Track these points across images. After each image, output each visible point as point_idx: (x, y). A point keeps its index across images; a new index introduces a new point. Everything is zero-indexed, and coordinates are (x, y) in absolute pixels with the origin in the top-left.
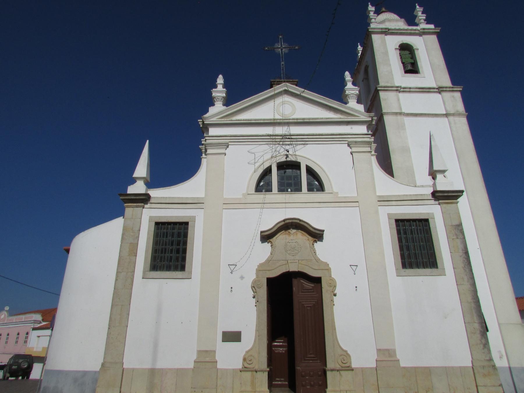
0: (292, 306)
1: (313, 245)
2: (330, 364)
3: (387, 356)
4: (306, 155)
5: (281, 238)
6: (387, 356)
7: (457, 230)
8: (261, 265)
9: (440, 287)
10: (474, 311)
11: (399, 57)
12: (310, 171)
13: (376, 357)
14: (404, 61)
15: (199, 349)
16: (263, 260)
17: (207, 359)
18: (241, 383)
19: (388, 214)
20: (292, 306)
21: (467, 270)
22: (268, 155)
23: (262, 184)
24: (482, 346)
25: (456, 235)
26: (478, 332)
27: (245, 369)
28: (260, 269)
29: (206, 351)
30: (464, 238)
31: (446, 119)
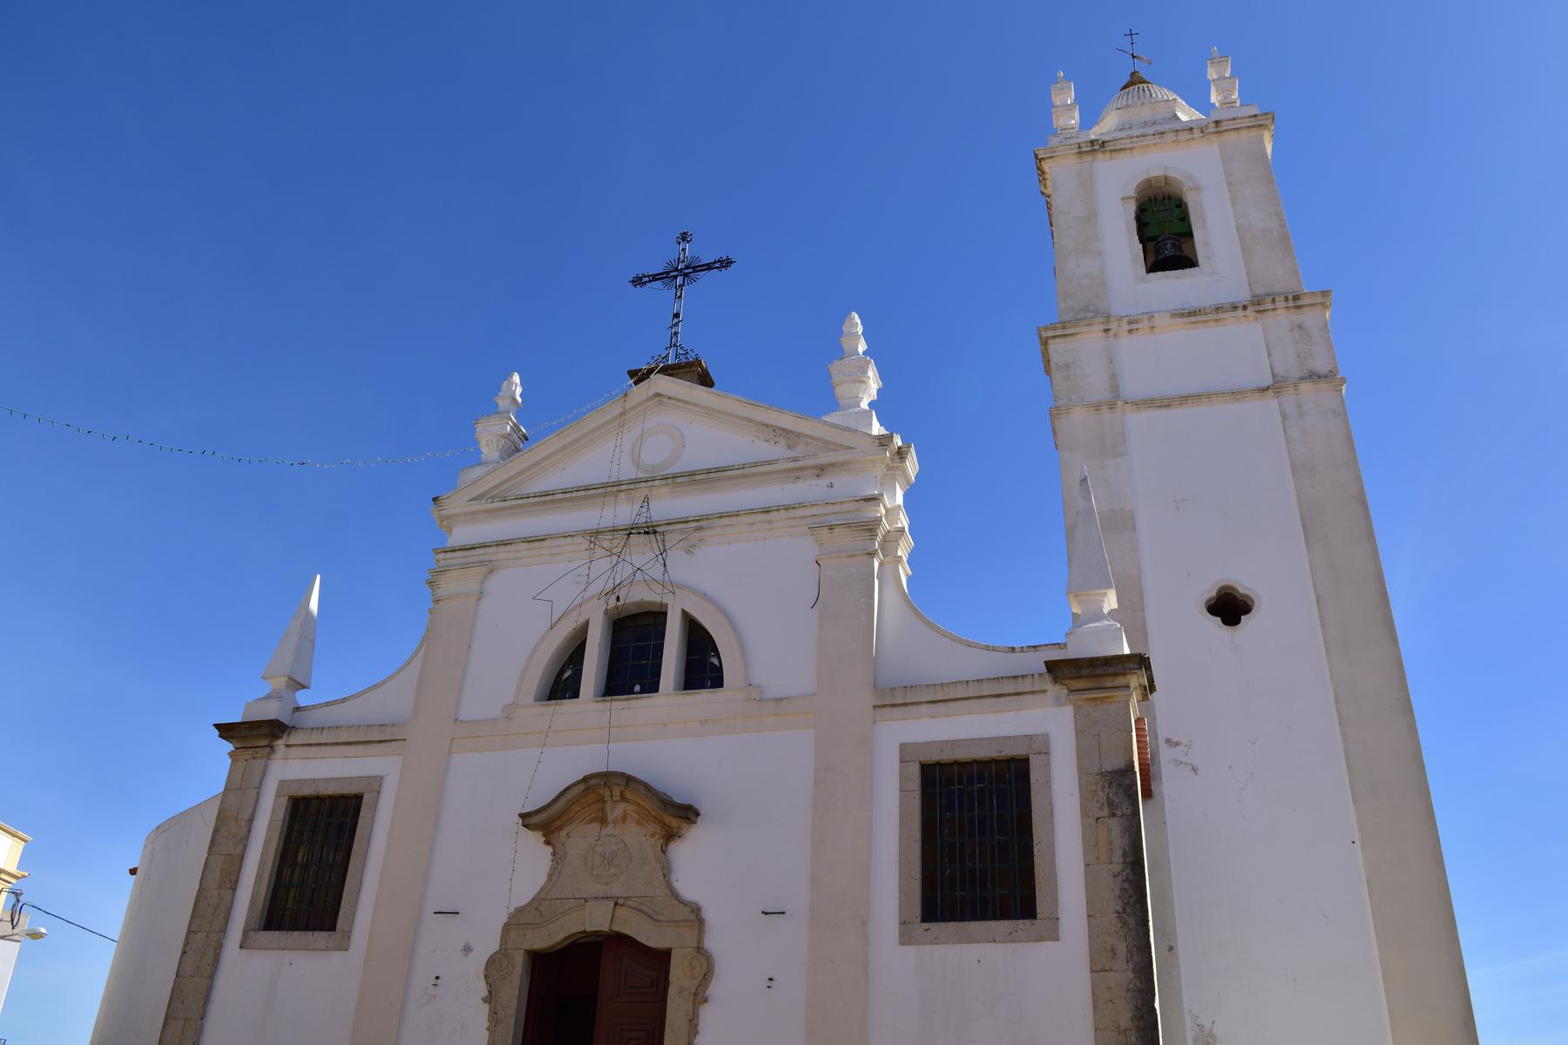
5: (581, 837)
11: (1134, 224)
14: (1151, 231)
21: (1132, 922)
23: (568, 674)
25: (1110, 804)
28: (516, 922)
31: (1275, 402)
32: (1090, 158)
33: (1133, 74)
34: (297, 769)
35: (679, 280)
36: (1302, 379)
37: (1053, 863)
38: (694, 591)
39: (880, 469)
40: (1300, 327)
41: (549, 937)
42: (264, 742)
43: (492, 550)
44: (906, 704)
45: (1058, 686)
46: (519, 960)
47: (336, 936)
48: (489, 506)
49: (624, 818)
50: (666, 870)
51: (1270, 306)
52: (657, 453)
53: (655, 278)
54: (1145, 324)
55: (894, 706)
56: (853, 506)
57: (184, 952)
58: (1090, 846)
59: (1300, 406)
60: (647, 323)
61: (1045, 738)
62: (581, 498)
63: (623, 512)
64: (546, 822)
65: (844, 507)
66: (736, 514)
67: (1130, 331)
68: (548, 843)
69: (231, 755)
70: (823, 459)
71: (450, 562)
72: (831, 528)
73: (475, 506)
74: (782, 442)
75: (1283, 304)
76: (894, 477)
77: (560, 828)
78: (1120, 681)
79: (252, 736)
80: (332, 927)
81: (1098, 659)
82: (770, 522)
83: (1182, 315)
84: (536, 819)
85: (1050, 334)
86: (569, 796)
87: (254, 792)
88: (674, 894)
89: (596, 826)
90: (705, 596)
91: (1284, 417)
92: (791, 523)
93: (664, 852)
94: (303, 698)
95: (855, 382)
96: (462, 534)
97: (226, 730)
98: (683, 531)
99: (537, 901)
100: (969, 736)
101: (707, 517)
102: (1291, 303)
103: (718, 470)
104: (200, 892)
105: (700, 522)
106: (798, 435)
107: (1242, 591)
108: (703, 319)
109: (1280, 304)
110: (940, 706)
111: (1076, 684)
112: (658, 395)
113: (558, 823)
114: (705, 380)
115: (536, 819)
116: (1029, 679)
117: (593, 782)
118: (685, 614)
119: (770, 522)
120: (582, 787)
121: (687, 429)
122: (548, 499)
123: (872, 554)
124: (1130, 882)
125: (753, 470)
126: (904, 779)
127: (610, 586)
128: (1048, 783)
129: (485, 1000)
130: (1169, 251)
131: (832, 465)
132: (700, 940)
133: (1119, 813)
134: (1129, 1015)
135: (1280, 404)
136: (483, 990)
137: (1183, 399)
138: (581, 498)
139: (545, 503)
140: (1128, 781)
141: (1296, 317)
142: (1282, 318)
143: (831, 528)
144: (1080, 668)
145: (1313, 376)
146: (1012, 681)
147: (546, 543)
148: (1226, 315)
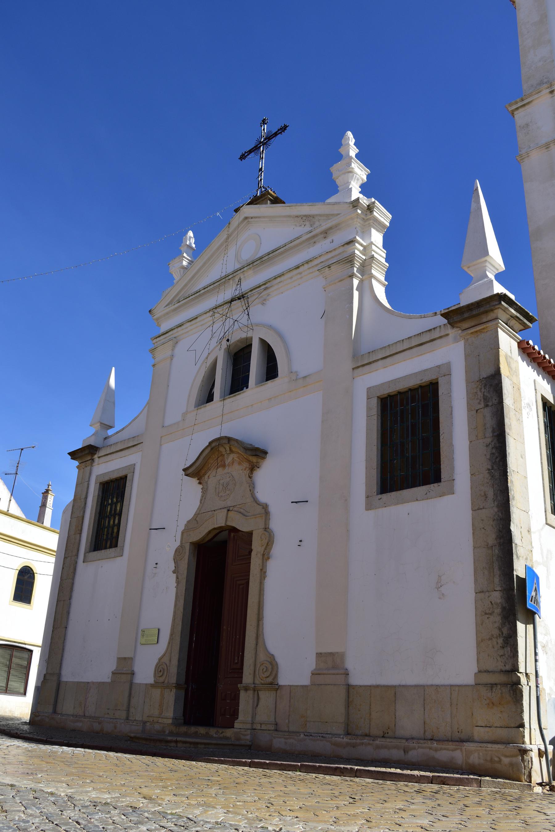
3: (330, 665)
5: (215, 477)
6: (330, 665)
9: (443, 515)
13: (313, 666)
15: (320, 651)
21: (497, 474)
24: (500, 641)
25: (486, 399)
26: (498, 611)
34: (105, 468)
39: (358, 223)
41: (198, 536)
42: (89, 458)
44: (370, 363)
45: (455, 329)
46: (187, 547)
47: (118, 549)
48: (173, 307)
50: (252, 487)
53: (250, 152)
56: (341, 249)
57: (63, 568)
58: (473, 429)
64: (196, 471)
65: (337, 252)
66: (282, 275)
68: (200, 483)
69: (78, 467)
70: (325, 225)
74: (307, 223)
76: (370, 226)
78: (491, 315)
79: (85, 454)
81: (472, 304)
82: (300, 273)
84: (190, 471)
86: (204, 454)
87: (86, 484)
88: (255, 500)
90: (270, 327)
92: (311, 270)
93: (250, 477)
94: (110, 432)
95: (344, 173)
97: (74, 455)
99: (197, 515)
100: (405, 374)
103: (273, 251)
104: (68, 537)
105: (265, 285)
106: (313, 216)
111: (465, 325)
112: (246, 218)
114: (276, 201)
115: (190, 471)
117: (213, 445)
120: (209, 449)
123: (352, 276)
125: (291, 245)
126: (369, 409)
129: (174, 572)
131: (331, 228)
133: (490, 404)
134: (494, 536)
136: (172, 566)
139: (196, 298)
146: (428, 333)
147: (198, 320)
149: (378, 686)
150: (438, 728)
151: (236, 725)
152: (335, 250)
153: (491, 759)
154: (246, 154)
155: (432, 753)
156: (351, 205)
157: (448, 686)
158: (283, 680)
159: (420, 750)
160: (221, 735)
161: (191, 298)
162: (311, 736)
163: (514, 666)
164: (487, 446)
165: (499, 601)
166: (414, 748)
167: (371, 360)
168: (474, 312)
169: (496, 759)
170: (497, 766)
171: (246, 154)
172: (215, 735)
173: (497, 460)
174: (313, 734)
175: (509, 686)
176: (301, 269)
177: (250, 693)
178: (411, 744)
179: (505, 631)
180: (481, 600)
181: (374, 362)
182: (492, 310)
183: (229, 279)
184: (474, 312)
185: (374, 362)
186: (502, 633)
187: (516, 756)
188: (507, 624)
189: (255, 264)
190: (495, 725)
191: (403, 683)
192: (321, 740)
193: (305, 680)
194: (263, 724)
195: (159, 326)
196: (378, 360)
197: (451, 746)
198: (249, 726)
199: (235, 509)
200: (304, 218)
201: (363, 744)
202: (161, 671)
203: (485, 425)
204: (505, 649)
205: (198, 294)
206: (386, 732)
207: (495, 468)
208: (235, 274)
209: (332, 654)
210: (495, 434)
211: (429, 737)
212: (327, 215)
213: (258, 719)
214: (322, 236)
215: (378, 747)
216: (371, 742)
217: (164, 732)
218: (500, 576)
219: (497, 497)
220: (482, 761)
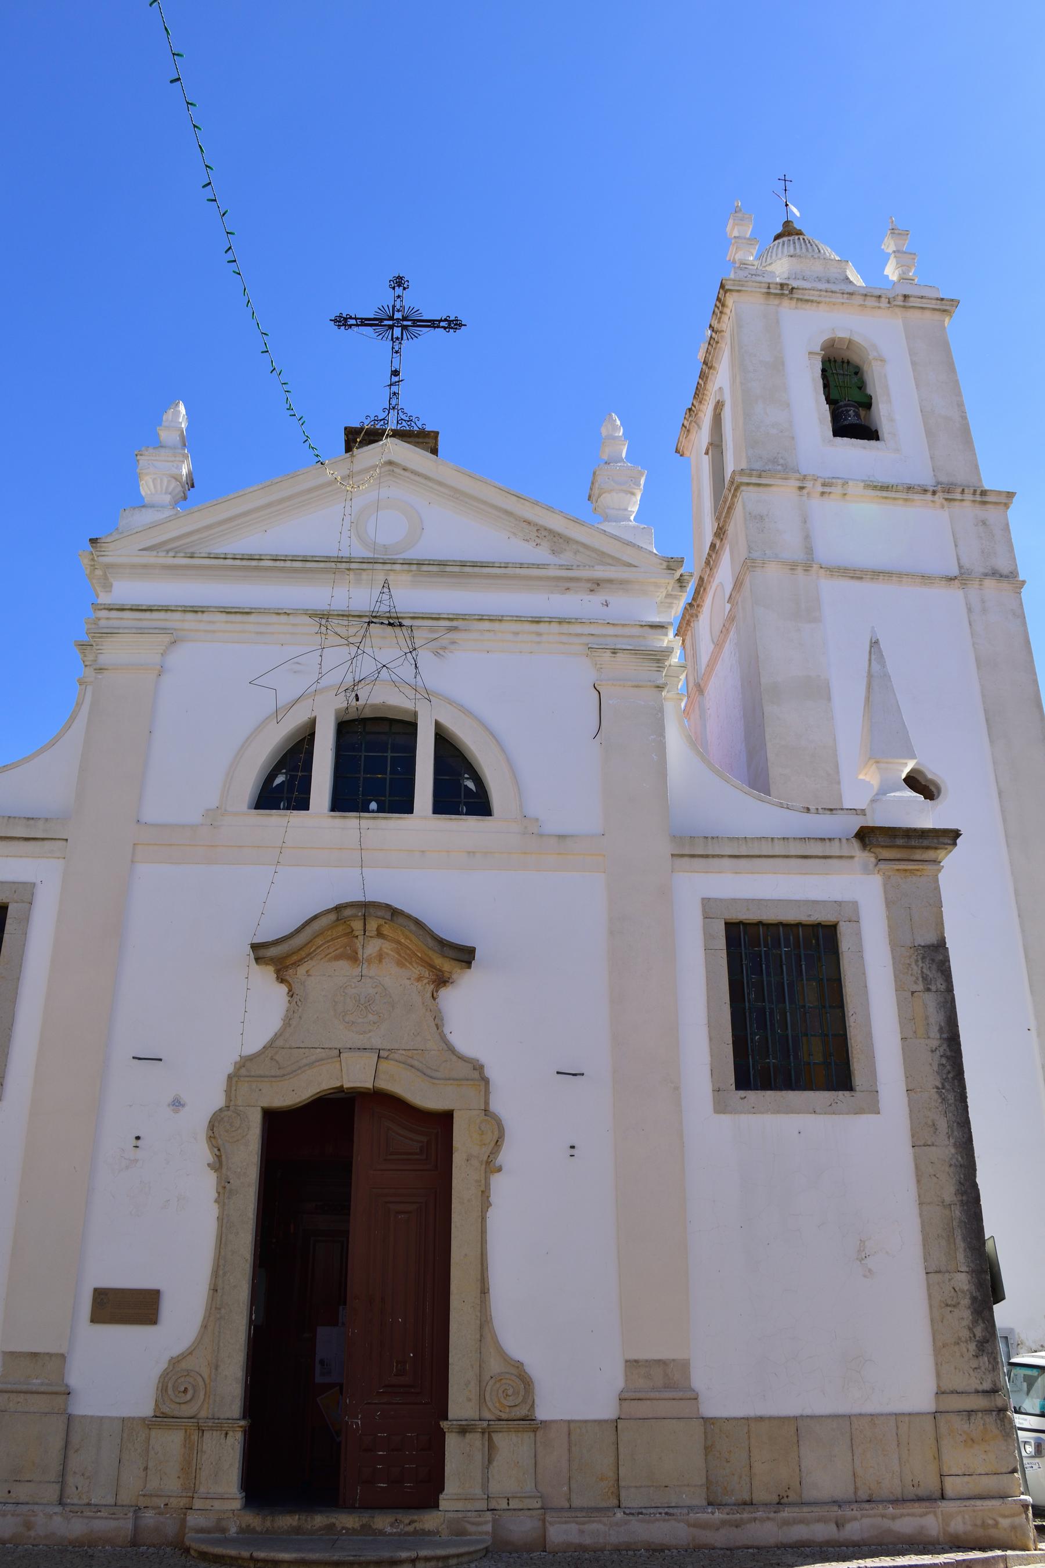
0: (348, 1202)
1: (434, 998)
2: (461, 1403)
3: (658, 1384)
4: (453, 691)
5: (324, 977)
7: (930, 965)
8: (245, 1063)
9: (855, 1150)
10: (958, 1234)
11: (820, 383)
12: (448, 750)
13: (620, 1383)
16: (254, 1045)
17: (36, 1383)
18: (146, 1469)
19: (706, 902)
20: (348, 1202)
21: (951, 1097)
22: (313, 685)
23: (280, 779)
24: (972, 1346)
25: (925, 978)
26: (966, 1301)
27: (161, 1419)
28: (244, 1072)
29: (35, 1355)
30: (950, 989)
31: (959, 594)
32: (776, 302)
33: (787, 223)
35: (397, 332)
36: (986, 575)
37: (869, 1035)
38: (451, 702)
40: (984, 523)
41: (294, 1092)
43: (177, 616)
44: (707, 856)
49: (381, 957)
51: (958, 496)
52: (388, 531)
53: (364, 322)
54: (837, 490)
55: (693, 856)
56: (636, 631)
58: (906, 1020)
59: (983, 602)
60: (358, 378)
61: (855, 904)
62: (295, 570)
63: (359, 595)
64: (278, 956)
65: (627, 631)
66: (500, 620)
67: (823, 494)
68: (281, 980)
70: (600, 572)
71: (116, 623)
72: (614, 652)
73: (149, 558)
75: (971, 498)
77: (297, 964)
78: (930, 854)
80: (744, 1080)
81: (915, 830)
82: (539, 634)
83: (875, 488)
84: (273, 952)
85: (746, 480)
86: (316, 926)
88: (451, 1049)
89: (343, 965)
91: (970, 610)
93: (434, 998)
96: (127, 590)
98: (432, 630)
101: (464, 617)
102: (978, 498)
105: (455, 622)
106: (568, 540)
107: (930, 776)
108: (430, 378)
109: (968, 496)
110: (743, 862)
111: (886, 854)
112: (390, 463)
113: (295, 958)
115: (273, 952)
116: (836, 843)
117: (348, 912)
118: (438, 725)
119: (539, 634)
121: (393, 506)
122: (251, 564)
124: (948, 1058)
125: (518, 571)
127: (349, 681)
128: (860, 952)
130: (851, 419)
131: (610, 581)
132: (487, 1103)
133: (933, 988)
134: (952, 1190)
135: (966, 597)
137: (876, 574)
138: (295, 570)
140: (941, 957)
141: (979, 512)
142: (967, 510)
143: (614, 652)
144: (895, 837)
145: (995, 574)
146: (819, 843)
147: (252, 618)
148: (916, 497)
149: (761, 1419)
150: (879, 1483)
151: (443, 1504)
152: (624, 625)
153: (983, 1522)
154: (353, 322)
155: (887, 1523)
156: (665, 564)
157: (890, 1414)
158: (549, 1408)
159: (866, 1521)
160: (410, 1528)
161: (229, 562)
162: (641, 1513)
163: (995, 1385)
164: (932, 1051)
165: (966, 1288)
166: (855, 1519)
167: (710, 853)
168: (913, 843)
169: (991, 1522)
170: (993, 1532)
171: (353, 322)
172: (388, 1530)
173: (950, 1076)
174: (644, 1511)
175: (994, 1413)
176: (542, 627)
177: (475, 1440)
178: (848, 1513)
179: (979, 1331)
180: (938, 1283)
181: (713, 856)
182: (936, 848)
183: (349, 569)
184: (913, 843)
185: (713, 856)
186: (975, 1336)
187: (1019, 1514)
188: (980, 1321)
189: (425, 568)
190: (979, 1472)
191: (808, 1412)
192: (664, 1520)
193: (605, 1409)
194: (514, 1497)
195: (107, 587)
196: (723, 856)
197: (917, 1508)
198: (482, 1505)
199: (396, 1056)
200: (545, 533)
201: (755, 1519)
202: (186, 1391)
203: (927, 1018)
204: (980, 1359)
205: (254, 563)
206: (785, 1495)
207: (948, 1087)
208: (365, 566)
209: (662, 1363)
210: (945, 1036)
211: (865, 1497)
212: (603, 553)
213: (494, 1487)
214: (589, 585)
215: (786, 1523)
216: (772, 1515)
217: (224, 1530)
218: (965, 1250)
219: (953, 1131)
220: (969, 1528)
